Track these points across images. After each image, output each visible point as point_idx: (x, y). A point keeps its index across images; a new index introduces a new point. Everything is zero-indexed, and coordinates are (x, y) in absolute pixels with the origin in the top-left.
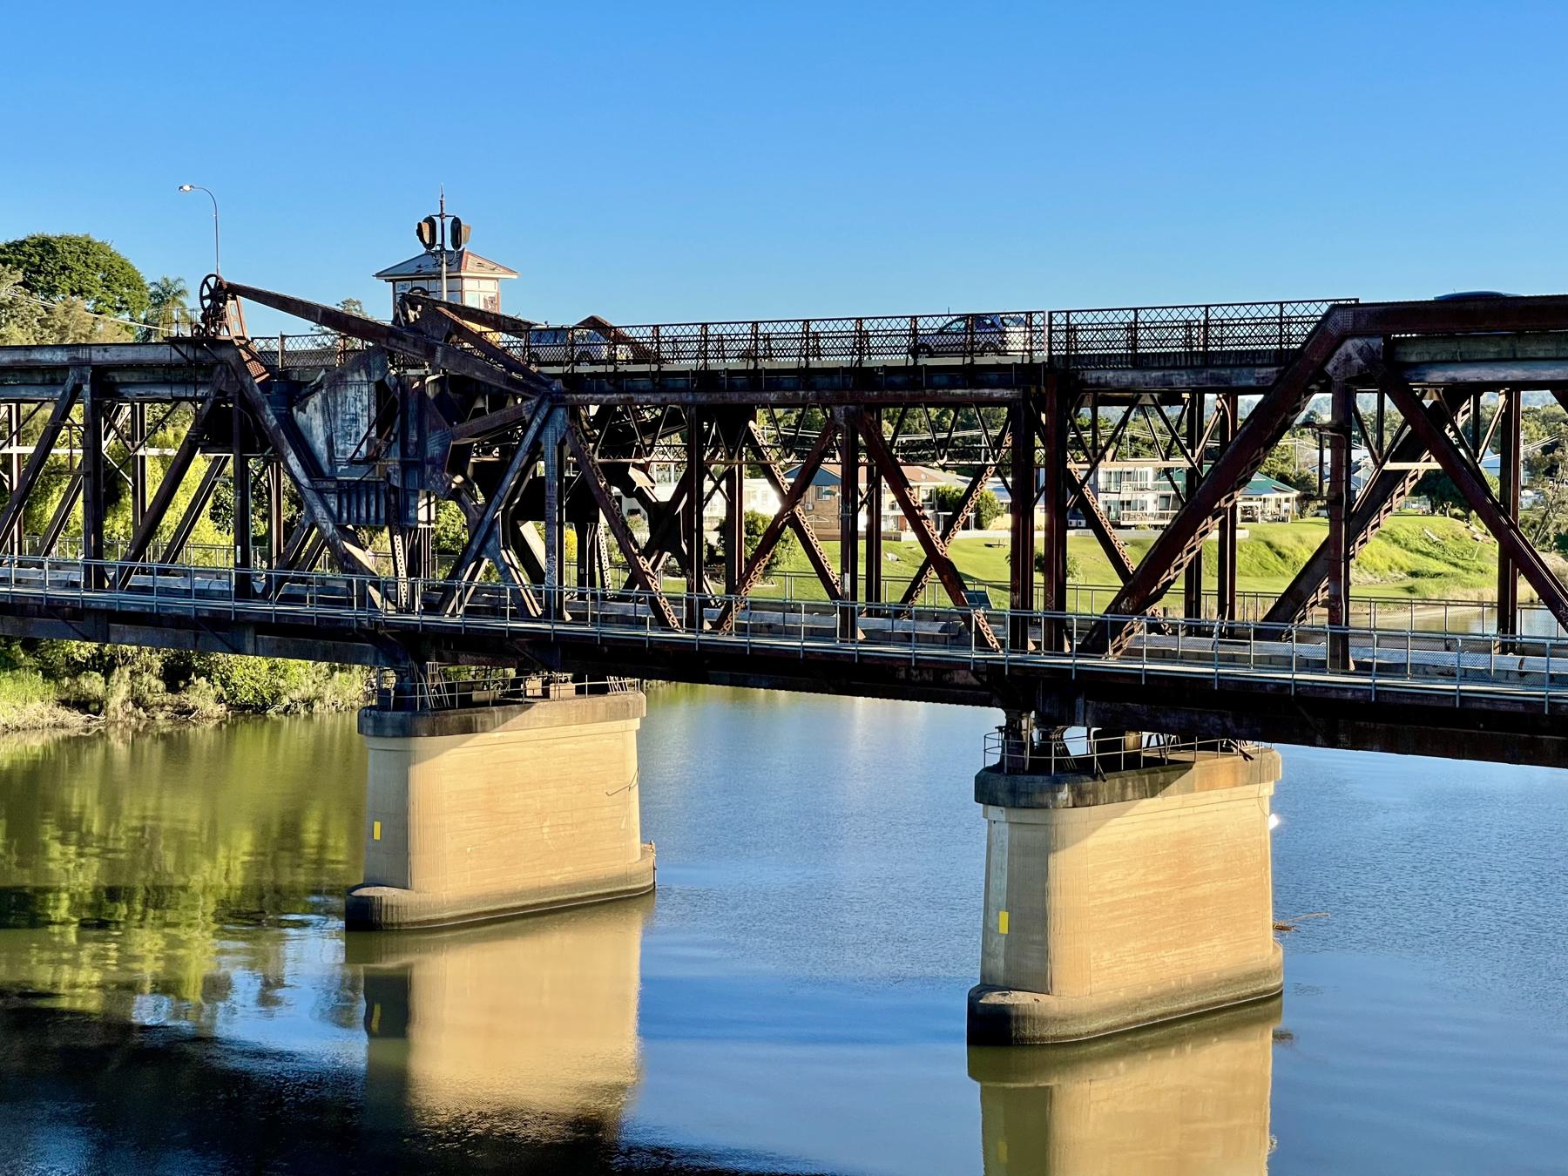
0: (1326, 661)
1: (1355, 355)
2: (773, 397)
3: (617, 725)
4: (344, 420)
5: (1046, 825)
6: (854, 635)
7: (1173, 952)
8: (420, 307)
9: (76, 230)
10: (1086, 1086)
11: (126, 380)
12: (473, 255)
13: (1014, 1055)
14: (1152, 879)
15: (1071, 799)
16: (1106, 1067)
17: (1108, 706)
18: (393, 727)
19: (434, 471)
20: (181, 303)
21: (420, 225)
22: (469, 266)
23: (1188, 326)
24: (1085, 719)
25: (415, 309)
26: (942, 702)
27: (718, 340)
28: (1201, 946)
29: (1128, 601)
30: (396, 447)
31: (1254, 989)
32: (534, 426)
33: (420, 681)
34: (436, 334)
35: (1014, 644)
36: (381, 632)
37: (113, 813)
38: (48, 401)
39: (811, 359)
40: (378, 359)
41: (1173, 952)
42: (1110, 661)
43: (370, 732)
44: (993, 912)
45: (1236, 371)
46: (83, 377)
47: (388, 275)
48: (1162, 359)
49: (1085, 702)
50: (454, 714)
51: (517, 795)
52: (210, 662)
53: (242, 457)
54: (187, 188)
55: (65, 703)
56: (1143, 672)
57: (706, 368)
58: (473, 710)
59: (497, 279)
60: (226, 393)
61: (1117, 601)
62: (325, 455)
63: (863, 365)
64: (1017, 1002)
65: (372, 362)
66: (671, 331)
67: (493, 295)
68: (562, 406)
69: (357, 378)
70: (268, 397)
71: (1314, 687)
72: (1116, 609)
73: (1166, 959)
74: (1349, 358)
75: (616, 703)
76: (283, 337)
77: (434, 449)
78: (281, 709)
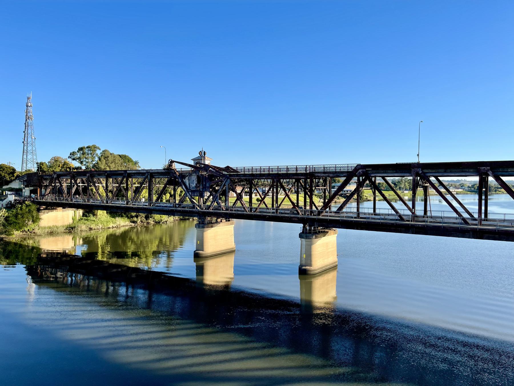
1: (361, 172)
2: (264, 178)
3: (232, 226)
9: (124, 154)
11: (155, 175)
13: (307, 276)
16: (319, 277)
19: (207, 188)
20: (138, 164)
26: (290, 223)
30: (201, 185)
35: (305, 214)
37: (138, 238)
42: (320, 217)
44: (302, 254)
45: (340, 174)
46: (148, 175)
47: (193, 160)
55: (131, 222)
61: (322, 208)
66: (263, 167)
69: (194, 174)
71: (357, 221)
74: (360, 172)
76: (181, 169)
77: (208, 185)
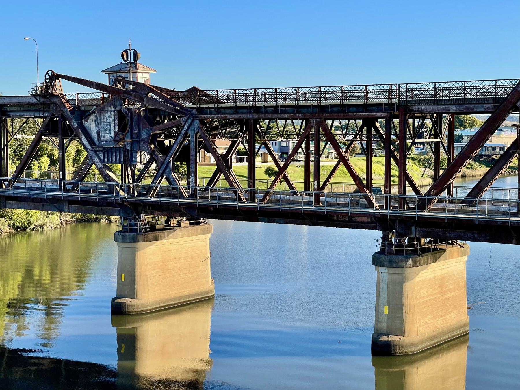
0: (313, 202)
2: (285, 116)
4: (104, 125)
5: (134, 248)
6: (319, 204)
7: (440, 319)
8: (122, 83)
10: (416, 369)
11: (12, 109)
12: (140, 64)
13: (392, 358)
14: (435, 292)
15: (412, 264)
17: (425, 229)
18: (129, 239)
19: (144, 144)
21: (122, 53)
22: (140, 68)
23: (246, 95)
24: (415, 234)
25: (120, 84)
27: (264, 95)
28: (448, 316)
29: (434, 191)
30: (129, 135)
31: (463, 331)
32: (186, 127)
33: (139, 222)
34: (143, 93)
35: (386, 207)
36: (125, 204)
38: (30, 117)
39: (278, 102)
40: (119, 102)
41: (440, 319)
42: (425, 213)
43: (120, 241)
45: (476, 106)
48: (446, 101)
49: (416, 228)
50: (151, 234)
51: (172, 263)
52: (5, 212)
53: (62, 139)
54: (27, 38)
56: (388, 214)
57: (256, 105)
58: (157, 232)
59: (149, 73)
60: (55, 114)
62: (97, 138)
63: (321, 104)
64: (393, 340)
65: (116, 103)
66: (282, 90)
67: (147, 79)
68: (197, 119)
69: (109, 109)
70: (73, 116)
72: (429, 194)
73: (438, 322)
75: (204, 228)
76: (78, 94)
78: (32, 228)
